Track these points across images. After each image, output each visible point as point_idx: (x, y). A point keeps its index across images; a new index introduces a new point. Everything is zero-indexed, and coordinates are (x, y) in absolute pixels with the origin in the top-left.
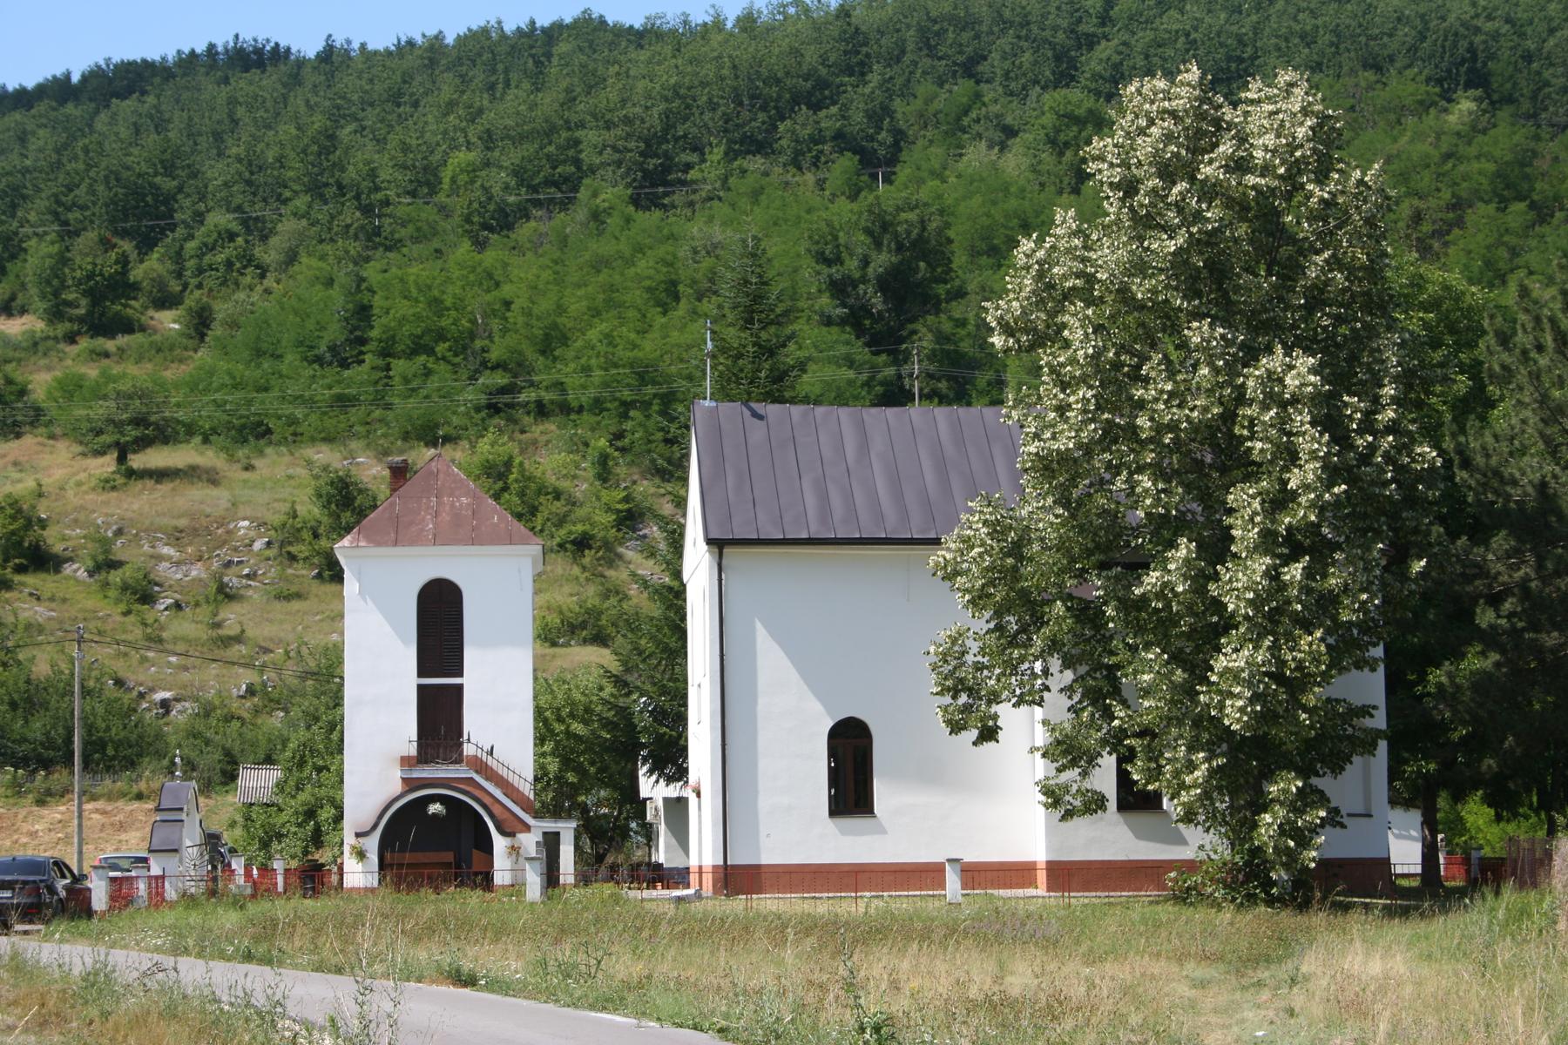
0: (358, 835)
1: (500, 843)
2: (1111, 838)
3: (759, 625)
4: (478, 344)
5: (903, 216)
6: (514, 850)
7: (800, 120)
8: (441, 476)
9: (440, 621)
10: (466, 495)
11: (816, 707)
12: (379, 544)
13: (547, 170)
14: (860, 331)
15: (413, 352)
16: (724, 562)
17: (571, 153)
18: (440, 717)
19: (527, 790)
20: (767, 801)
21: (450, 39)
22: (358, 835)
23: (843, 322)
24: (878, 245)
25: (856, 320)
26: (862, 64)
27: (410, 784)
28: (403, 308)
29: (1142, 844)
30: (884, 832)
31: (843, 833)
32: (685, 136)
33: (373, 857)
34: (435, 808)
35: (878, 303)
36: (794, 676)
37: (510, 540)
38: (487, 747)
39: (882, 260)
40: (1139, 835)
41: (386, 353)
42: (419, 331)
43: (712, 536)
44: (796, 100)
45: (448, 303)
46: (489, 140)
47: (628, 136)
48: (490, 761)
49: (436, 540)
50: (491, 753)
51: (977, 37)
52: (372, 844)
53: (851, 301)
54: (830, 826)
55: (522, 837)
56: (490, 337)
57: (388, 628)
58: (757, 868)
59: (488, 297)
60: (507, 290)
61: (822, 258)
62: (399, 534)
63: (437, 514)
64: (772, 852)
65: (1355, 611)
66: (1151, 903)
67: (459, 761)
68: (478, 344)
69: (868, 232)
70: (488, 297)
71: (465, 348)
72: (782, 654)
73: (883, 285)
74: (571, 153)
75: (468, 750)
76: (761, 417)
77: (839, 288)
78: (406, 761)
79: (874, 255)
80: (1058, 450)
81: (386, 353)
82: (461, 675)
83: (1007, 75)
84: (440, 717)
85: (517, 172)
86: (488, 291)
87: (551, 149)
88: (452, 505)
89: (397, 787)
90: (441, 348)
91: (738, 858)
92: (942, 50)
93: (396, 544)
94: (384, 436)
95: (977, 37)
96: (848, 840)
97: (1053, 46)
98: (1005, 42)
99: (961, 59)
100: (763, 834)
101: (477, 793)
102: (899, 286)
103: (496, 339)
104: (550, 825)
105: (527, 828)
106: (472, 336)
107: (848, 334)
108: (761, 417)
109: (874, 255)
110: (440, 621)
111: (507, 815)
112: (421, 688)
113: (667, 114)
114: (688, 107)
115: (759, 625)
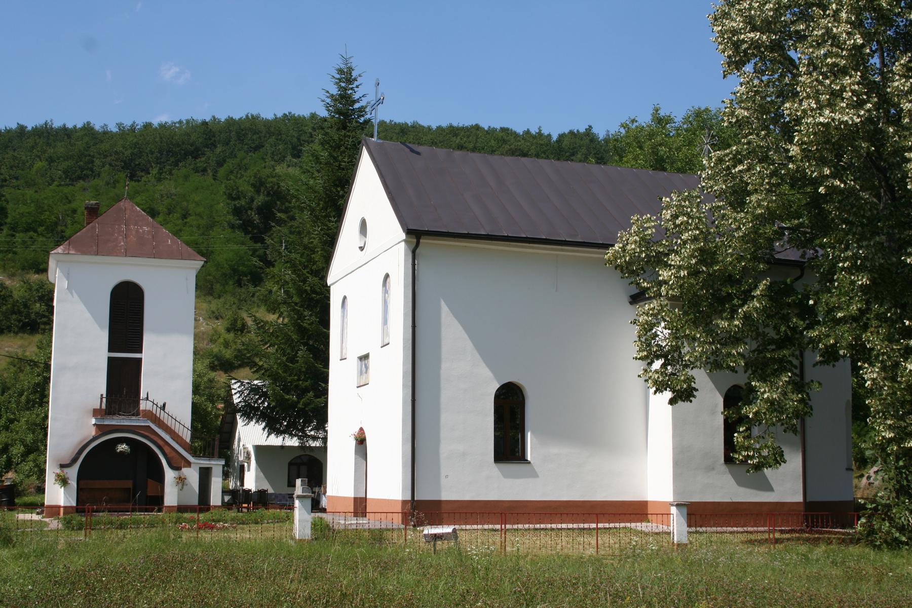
0: (62, 466)
1: (170, 475)
2: (725, 489)
3: (443, 303)
4: (59, 228)
5: (271, 179)
6: (181, 481)
7: (188, 162)
8: (128, 212)
9: (126, 315)
10: (147, 225)
11: (485, 372)
12: (84, 253)
13: (79, 172)
14: (247, 232)
15: (26, 230)
16: (418, 251)
17: (90, 165)
18: (123, 380)
19: (187, 436)
20: (447, 448)
21: (30, 128)
22: (62, 466)
23: (240, 227)
24: (258, 192)
25: (246, 226)
26: (212, 144)
27: (102, 429)
28: (23, 209)
29: (742, 489)
30: (534, 475)
31: (506, 476)
32: (139, 164)
33: (73, 483)
34: (122, 447)
35: (256, 218)
36: (469, 345)
37: (182, 257)
38: (160, 404)
39: (260, 199)
40: (740, 483)
41: (14, 228)
42: (30, 221)
43: (411, 227)
44: (187, 154)
45: (46, 208)
46: (51, 160)
47: (117, 160)
48: (163, 416)
49: (127, 254)
50: (163, 407)
51: (260, 138)
52: (72, 473)
53: (244, 217)
54: (494, 470)
55: (185, 471)
56: (66, 226)
57: (88, 315)
58: (438, 503)
59: (66, 207)
60: (73, 205)
61: (231, 197)
62: (100, 247)
63: (126, 236)
64: (452, 489)
65: (710, 343)
66: (751, 542)
67: (137, 414)
68: (59, 228)
69: (253, 185)
70: (66, 207)
71: (52, 230)
72: (461, 328)
73: (260, 211)
74: (90, 165)
75: (143, 406)
76: (418, 153)
77: (237, 212)
78: (96, 413)
79: (256, 196)
80: (846, 123)
81: (14, 228)
82: (141, 352)
83: (273, 153)
84: (123, 380)
85: (65, 172)
86: (64, 204)
87: (82, 163)
88: (137, 231)
89: (93, 432)
90: (41, 229)
91: (423, 495)
92: (246, 141)
93: (97, 254)
94: (13, 267)
95: (260, 138)
96: (509, 482)
97: (291, 144)
98: (272, 140)
99: (253, 146)
100: (443, 473)
101: (156, 439)
102: (266, 212)
103: (69, 226)
104: (205, 463)
105: (189, 464)
106: (56, 224)
107: (239, 234)
108: (418, 153)
109: (256, 196)
110: (126, 315)
111: (174, 454)
112: (110, 359)
113: (132, 154)
114: (141, 152)
115: (443, 303)
